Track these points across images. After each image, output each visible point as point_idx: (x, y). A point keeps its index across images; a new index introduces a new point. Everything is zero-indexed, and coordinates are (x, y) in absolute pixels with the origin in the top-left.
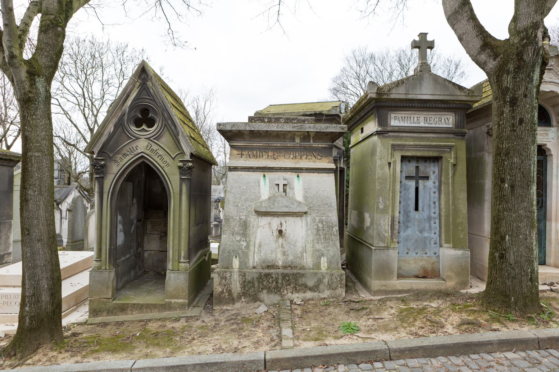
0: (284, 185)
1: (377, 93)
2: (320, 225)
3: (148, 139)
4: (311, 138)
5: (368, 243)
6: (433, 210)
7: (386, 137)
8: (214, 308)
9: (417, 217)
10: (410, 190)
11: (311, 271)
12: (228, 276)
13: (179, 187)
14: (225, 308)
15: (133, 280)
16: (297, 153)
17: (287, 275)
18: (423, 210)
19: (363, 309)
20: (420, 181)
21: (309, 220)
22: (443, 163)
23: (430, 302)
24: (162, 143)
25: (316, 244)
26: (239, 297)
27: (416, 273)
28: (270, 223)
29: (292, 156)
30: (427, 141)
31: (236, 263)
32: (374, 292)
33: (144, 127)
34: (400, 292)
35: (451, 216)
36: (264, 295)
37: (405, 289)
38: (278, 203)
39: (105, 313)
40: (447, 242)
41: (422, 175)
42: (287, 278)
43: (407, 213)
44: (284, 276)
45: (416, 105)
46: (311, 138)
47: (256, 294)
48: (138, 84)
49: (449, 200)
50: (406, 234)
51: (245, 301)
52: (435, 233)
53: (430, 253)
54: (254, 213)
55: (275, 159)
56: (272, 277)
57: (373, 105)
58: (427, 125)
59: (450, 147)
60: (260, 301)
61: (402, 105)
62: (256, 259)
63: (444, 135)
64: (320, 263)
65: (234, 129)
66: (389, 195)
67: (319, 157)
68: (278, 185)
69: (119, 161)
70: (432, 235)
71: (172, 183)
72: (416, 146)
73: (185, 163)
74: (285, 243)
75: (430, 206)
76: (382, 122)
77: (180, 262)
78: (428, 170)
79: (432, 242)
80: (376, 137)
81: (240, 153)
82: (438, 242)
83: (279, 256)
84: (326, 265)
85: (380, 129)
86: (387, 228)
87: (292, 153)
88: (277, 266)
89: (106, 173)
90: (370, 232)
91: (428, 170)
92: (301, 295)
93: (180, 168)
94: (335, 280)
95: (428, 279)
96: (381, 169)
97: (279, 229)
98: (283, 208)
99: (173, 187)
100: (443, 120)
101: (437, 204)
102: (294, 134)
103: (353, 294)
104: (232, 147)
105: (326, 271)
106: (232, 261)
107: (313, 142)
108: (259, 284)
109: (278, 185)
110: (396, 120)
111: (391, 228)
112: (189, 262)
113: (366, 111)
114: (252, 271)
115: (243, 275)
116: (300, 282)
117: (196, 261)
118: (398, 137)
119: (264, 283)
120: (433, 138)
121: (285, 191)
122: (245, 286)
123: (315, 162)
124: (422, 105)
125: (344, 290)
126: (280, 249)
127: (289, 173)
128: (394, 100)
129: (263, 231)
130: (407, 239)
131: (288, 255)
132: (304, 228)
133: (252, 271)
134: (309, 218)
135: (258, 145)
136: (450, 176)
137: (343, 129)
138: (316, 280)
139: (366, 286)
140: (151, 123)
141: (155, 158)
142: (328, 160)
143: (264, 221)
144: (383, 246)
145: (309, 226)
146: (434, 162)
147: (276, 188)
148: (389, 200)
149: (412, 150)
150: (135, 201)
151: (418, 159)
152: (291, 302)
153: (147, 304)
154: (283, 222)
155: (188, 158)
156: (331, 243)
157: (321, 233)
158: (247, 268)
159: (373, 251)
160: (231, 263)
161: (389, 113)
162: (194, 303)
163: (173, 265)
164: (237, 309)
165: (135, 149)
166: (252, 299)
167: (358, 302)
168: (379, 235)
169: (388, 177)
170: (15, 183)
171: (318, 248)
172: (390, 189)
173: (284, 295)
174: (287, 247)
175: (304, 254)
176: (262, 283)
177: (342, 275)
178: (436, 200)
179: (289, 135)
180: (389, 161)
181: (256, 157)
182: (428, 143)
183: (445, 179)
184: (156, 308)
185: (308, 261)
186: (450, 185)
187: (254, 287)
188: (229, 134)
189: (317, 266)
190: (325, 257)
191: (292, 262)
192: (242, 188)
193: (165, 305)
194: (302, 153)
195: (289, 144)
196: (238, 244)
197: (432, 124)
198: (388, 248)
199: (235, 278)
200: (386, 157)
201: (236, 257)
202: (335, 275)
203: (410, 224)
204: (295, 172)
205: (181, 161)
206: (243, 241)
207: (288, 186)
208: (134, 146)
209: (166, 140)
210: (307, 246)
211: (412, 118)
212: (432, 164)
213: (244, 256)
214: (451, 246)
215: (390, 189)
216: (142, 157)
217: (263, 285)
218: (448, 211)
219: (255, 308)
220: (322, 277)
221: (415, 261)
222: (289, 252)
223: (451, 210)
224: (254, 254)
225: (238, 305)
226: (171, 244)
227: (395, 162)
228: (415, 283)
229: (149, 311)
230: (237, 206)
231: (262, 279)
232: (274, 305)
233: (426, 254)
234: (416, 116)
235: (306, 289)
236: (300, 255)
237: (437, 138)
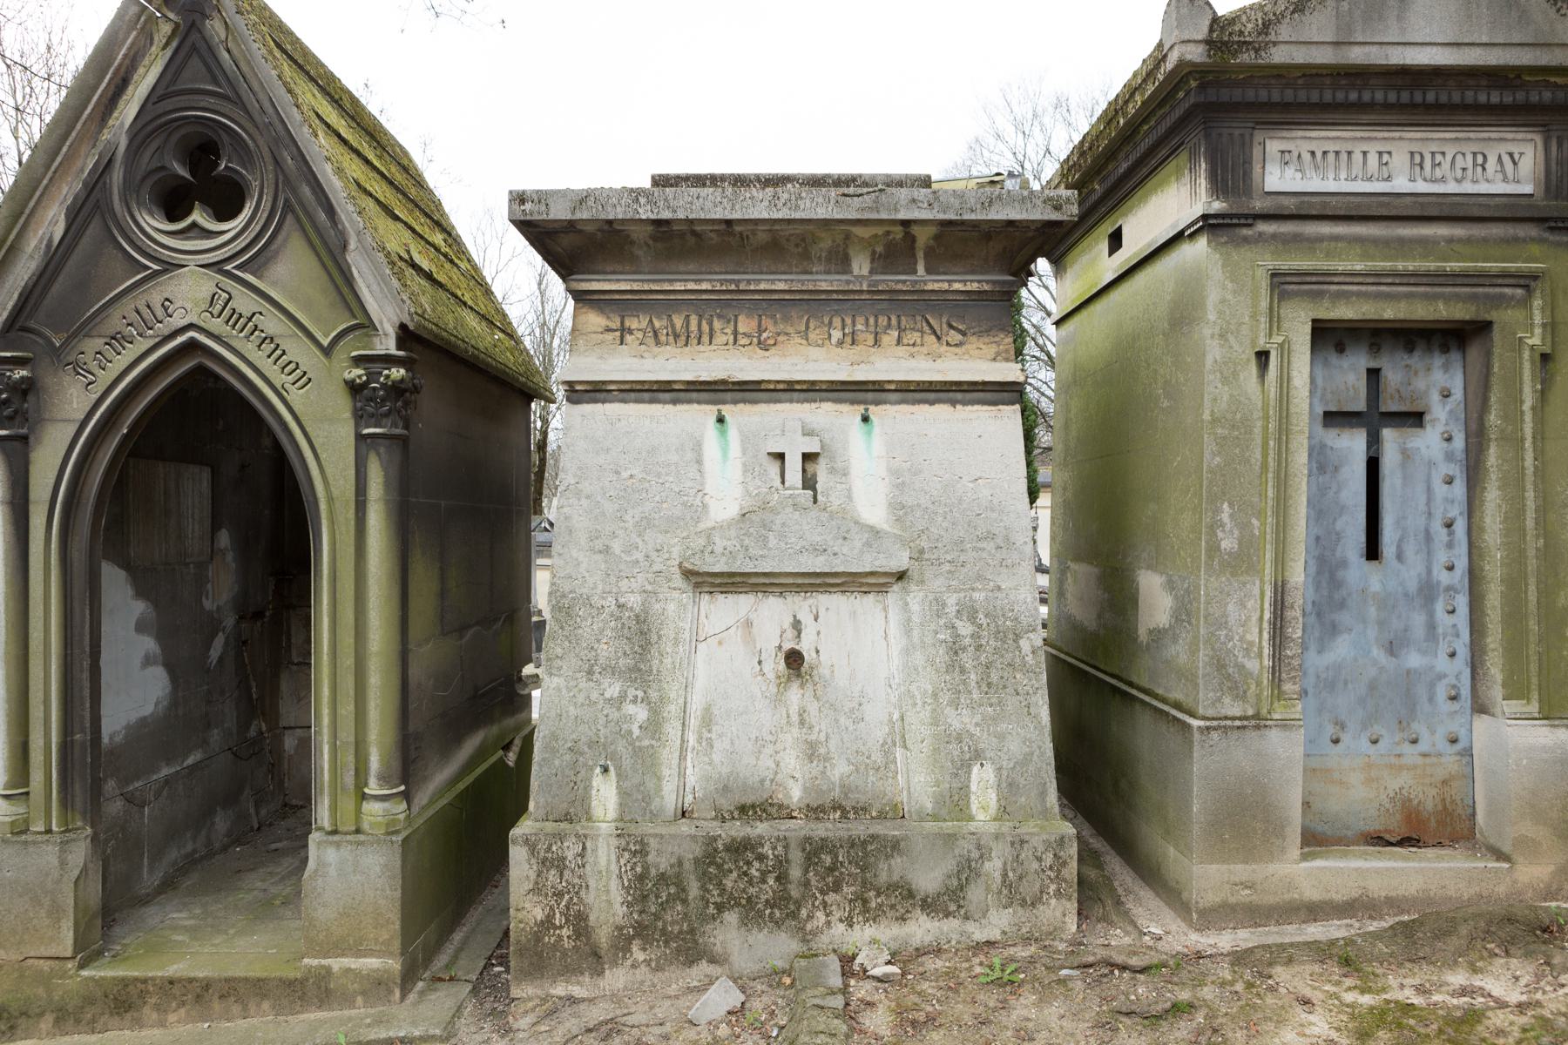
0: (808, 457)
1: (1208, 42)
2: (965, 629)
3: (216, 266)
4: (920, 255)
5: (1164, 700)
6: (1442, 557)
7: (1246, 240)
8: (515, 992)
9: (1375, 585)
10: (1345, 472)
11: (930, 826)
12: (570, 855)
13: (352, 472)
14: (560, 990)
15: (225, 849)
16: (860, 320)
17: (824, 845)
18: (1400, 557)
19: (1177, 1010)
20: (1388, 434)
21: (915, 607)
22: (1497, 351)
23: (1475, 970)
24: (274, 284)
26: (622, 944)
27: (1374, 826)
28: (749, 624)
29: (836, 334)
30: (1424, 257)
31: (605, 797)
32: (1203, 913)
33: (198, 216)
34: (1315, 911)
35: (1532, 581)
36: (728, 934)
37: (1338, 897)
38: (782, 536)
39: (46, 1023)
40: (1515, 690)
41: (1394, 408)
42: (828, 860)
43: (1327, 569)
44: (814, 850)
45: (1379, 96)
46: (920, 255)
47: (692, 931)
48: (166, 29)
49: (1523, 509)
50: (1330, 657)
51: (647, 962)
52: (1452, 655)
53: (1433, 739)
54: (678, 581)
55: (763, 346)
56: (761, 858)
57: (1192, 100)
58: (1421, 187)
59: (1527, 281)
60: (713, 960)
61: (1315, 97)
62: (692, 779)
63: (1496, 230)
65: (584, 215)
66: (1263, 495)
67: (955, 337)
68: (781, 457)
69: (93, 366)
70: (1442, 663)
71: (323, 456)
72: (1377, 277)
73: (375, 367)
74: (813, 707)
75: (1429, 536)
76: (1230, 175)
77: (364, 797)
78: (1420, 384)
79: (1442, 692)
80: (1202, 242)
81: (615, 324)
82: (1465, 692)
83: (792, 762)
84: (992, 798)
85: (1217, 206)
86: (1253, 636)
87: (837, 321)
88: (781, 806)
89: (40, 421)
90: (1178, 651)
91: (1420, 384)
92: (887, 932)
93: (354, 388)
94: (1035, 865)
95: (1430, 852)
96: (1225, 381)
97: (787, 646)
98: (803, 558)
99: (329, 471)
100: (1492, 164)
101: (1460, 527)
102: (848, 236)
103: (1111, 923)
104: (580, 297)
105: (992, 828)
106: (588, 788)
107: (929, 271)
108: (704, 888)
109: (781, 457)
110: (1290, 167)
111: (1273, 638)
112: (407, 796)
113: (1148, 142)
114: (673, 830)
115: (635, 848)
116: (883, 878)
117: (431, 802)
118: (1297, 238)
119: (728, 883)
120: (1450, 240)
121: (809, 483)
122: (645, 897)
123: (936, 357)
124: (1405, 97)
125: (1073, 906)
126: (795, 731)
127: (828, 406)
128: (1283, 74)
129: (720, 651)
130: (1331, 682)
131: (827, 759)
132: (897, 641)
133: (673, 830)
134: (916, 598)
135: (691, 286)
136: (1527, 406)
137: (1057, 208)
138: (950, 865)
139: (1150, 874)
140: (227, 202)
141: (249, 349)
142: (993, 349)
143: (725, 610)
144: (1237, 712)
145: (915, 633)
146: (1445, 349)
147: (774, 469)
148: (1260, 514)
149: (1359, 294)
150: (224, 538)
151: (1377, 336)
152: (847, 960)
153: (227, 980)
154: (806, 618)
155: (387, 344)
156: (1012, 703)
157: (967, 659)
158: (654, 817)
159: (1197, 736)
160: (585, 800)
161: (1259, 136)
162: (442, 960)
163: (334, 808)
164: (615, 998)
165: (160, 312)
166: (678, 950)
167: (1143, 971)
168: (1220, 665)
169: (1257, 414)
171: (956, 725)
172: (1264, 466)
173: (816, 933)
174: (821, 725)
175: (899, 753)
176: (720, 883)
177: (1061, 841)
178: (1457, 512)
179: (826, 244)
180: (1262, 344)
181: (682, 338)
182: (1432, 265)
183: (1505, 418)
184: (264, 996)
185: (915, 782)
186: (1528, 444)
187: (684, 901)
188: (566, 241)
189: (956, 803)
190: (989, 767)
191: (846, 789)
192: (639, 474)
193: (303, 982)
194: (883, 321)
195: (826, 282)
196: (615, 715)
197: (1443, 179)
198: (1258, 721)
199: (603, 861)
200: (1245, 330)
201: (606, 770)
202: (1036, 841)
203: (1344, 618)
204: (853, 402)
205: (358, 361)
206: (634, 701)
207: (822, 461)
208: (156, 299)
209: (293, 271)
210: (911, 717)
211: (1358, 157)
212: (1438, 360)
213: (637, 763)
214: (1534, 708)
215: (1264, 466)
216: (192, 346)
217: (723, 891)
218: (1516, 557)
219: (690, 990)
220: (975, 854)
221: (1368, 780)
222: (832, 744)
223: (1531, 553)
224: (682, 758)
225: (616, 978)
226: (326, 721)
227: (1286, 348)
228: (1377, 871)
229: (236, 1009)
230: (606, 550)
231: (719, 867)
232: (773, 977)
233: (1415, 742)
234: (1373, 149)
235: (907, 904)
236: (877, 757)
237: (1468, 241)
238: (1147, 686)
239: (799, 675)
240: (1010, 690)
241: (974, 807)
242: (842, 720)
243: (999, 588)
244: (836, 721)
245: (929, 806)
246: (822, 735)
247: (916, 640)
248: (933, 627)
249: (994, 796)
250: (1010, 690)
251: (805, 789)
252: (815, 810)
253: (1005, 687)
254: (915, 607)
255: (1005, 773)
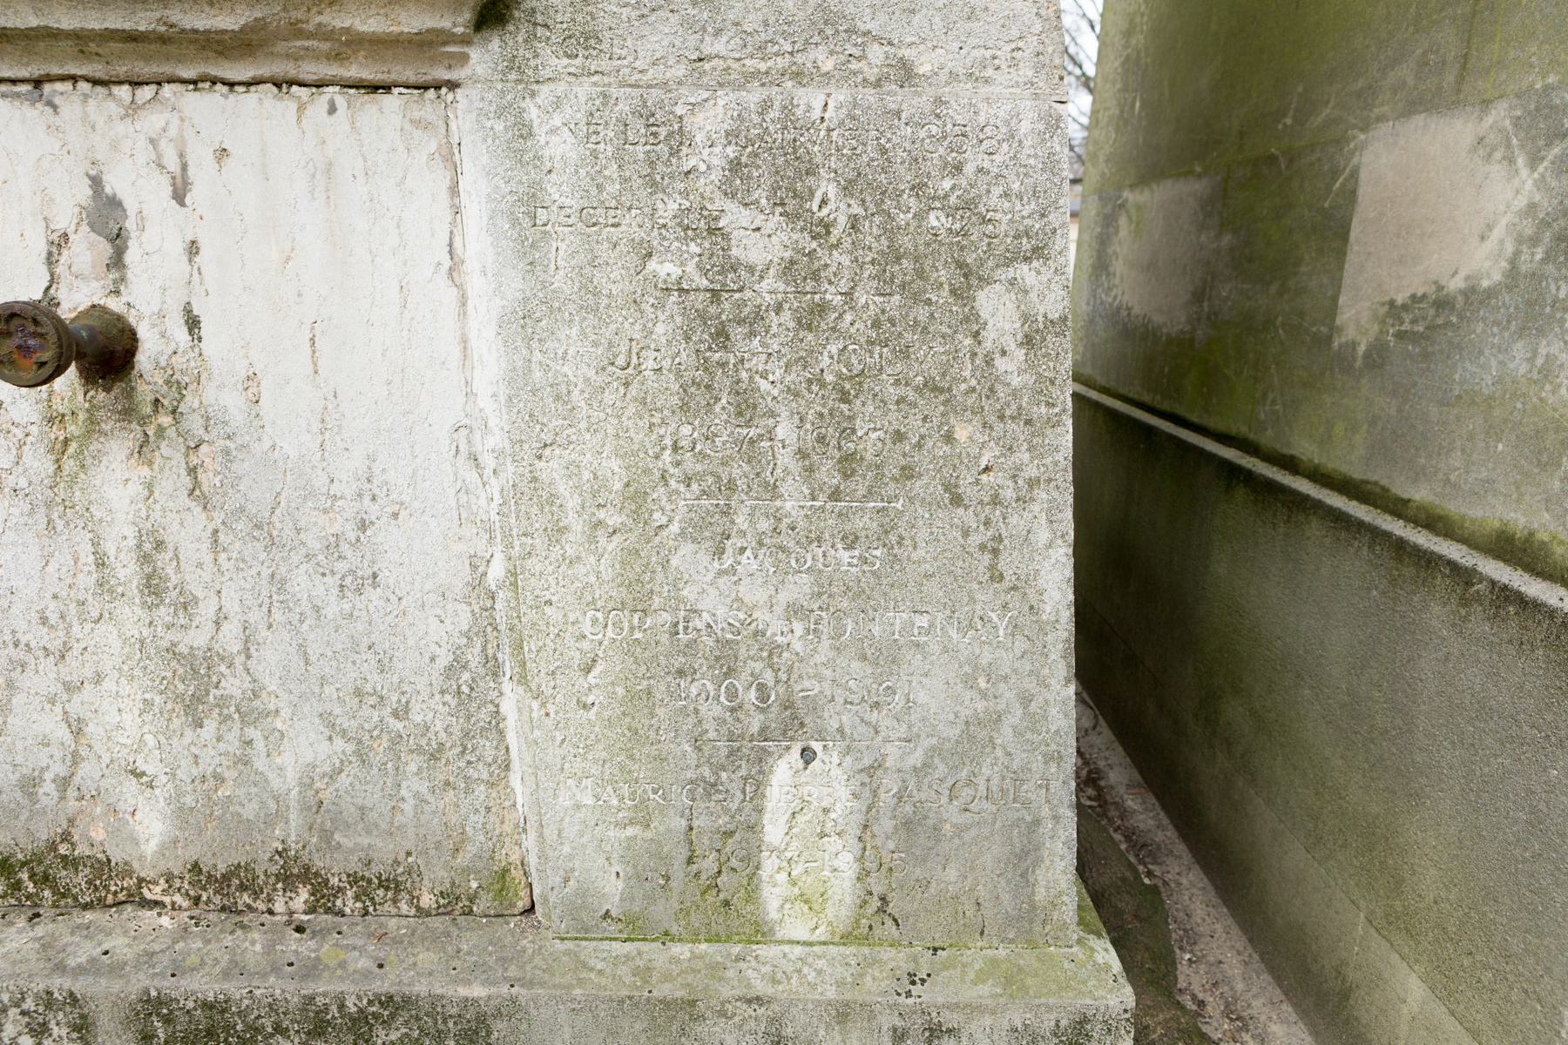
2: (761, 240)
21: (560, 146)
25: (690, 559)
64: (740, 841)
74: (188, 532)
83: (123, 717)
84: (840, 869)
88: (103, 868)
126: (131, 615)
145: (564, 248)
156: (933, 536)
170: (1364, 508)
174: (224, 595)
189: (711, 886)
190: (829, 760)
222: (271, 660)
236: (433, 713)
238: (1356, 472)
239: (128, 413)
240: (927, 485)
241: (774, 894)
242: (302, 582)
243: (905, 73)
244: (279, 582)
245: (612, 889)
246: (231, 630)
247: (560, 281)
248: (632, 226)
249: (846, 862)
250: (927, 485)
251: (181, 814)
252: (223, 882)
253: (908, 473)
254: (560, 146)
255: (890, 784)
